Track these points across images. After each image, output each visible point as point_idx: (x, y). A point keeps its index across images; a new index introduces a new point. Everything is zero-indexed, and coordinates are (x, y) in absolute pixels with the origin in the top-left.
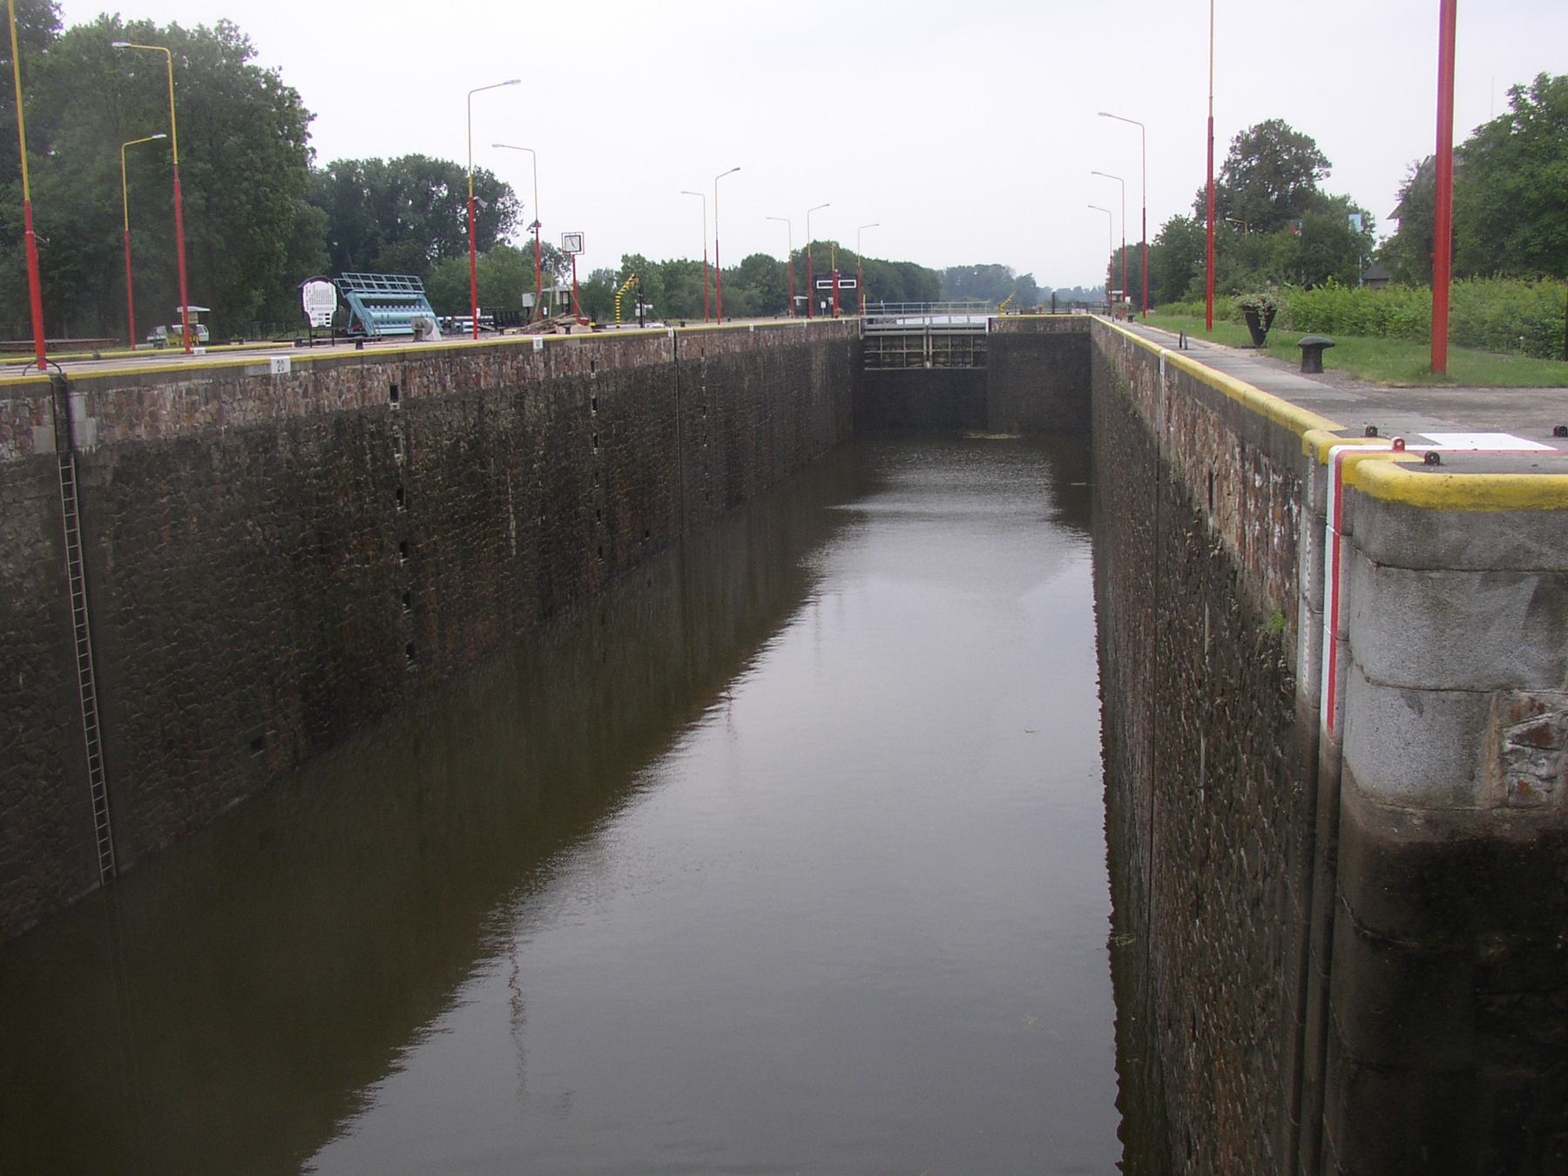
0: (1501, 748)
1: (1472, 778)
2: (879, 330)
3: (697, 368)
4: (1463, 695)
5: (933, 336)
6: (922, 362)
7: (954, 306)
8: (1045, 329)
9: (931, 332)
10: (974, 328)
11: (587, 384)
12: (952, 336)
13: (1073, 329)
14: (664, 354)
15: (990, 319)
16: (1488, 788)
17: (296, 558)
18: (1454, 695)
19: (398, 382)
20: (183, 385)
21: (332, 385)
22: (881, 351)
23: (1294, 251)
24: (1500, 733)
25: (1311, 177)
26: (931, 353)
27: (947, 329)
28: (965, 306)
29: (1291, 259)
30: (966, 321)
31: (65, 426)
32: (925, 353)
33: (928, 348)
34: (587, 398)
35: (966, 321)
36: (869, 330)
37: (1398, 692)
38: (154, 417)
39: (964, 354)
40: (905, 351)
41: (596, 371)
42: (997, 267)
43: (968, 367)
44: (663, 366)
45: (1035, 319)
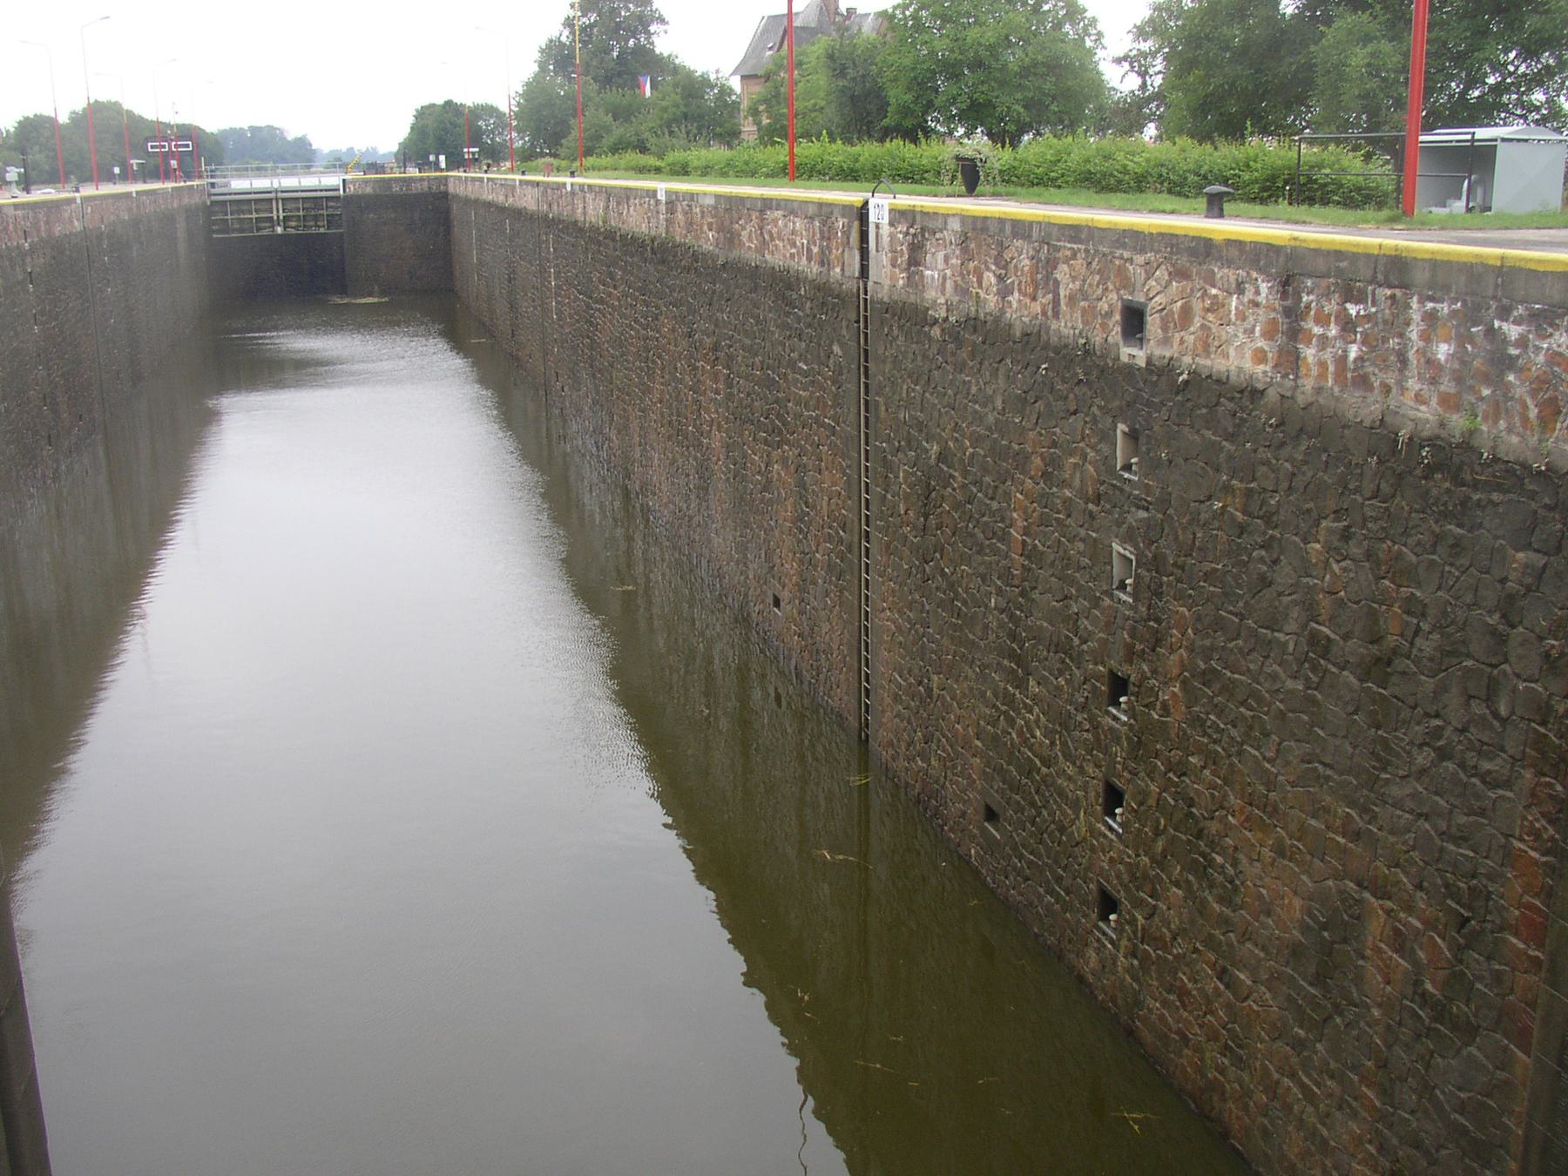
2: (225, 194)
3: (100, 237)
5: (283, 199)
6: (273, 227)
7: (236, 170)
8: (402, 190)
9: (280, 195)
10: (326, 190)
11: (23, 254)
12: (303, 198)
13: (430, 188)
14: (76, 223)
15: (344, 180)
22: (229, 217)
23: (677, 106)
25: (649, 34)
26: (281, 217)
27: (297, 191)
28: (247, 169)
29: (674, 114)
30: (317, 183)
32: (275, 218)
33: (278, 213)
34: (25, 271)
35: (317, 183)
36: (215, 195)
39: (316, 218)
40: (254, 215)
41: (29, 240)
42: (271, 128)
43: (322, 230)
44: (76, 235)
45: (390, 179)
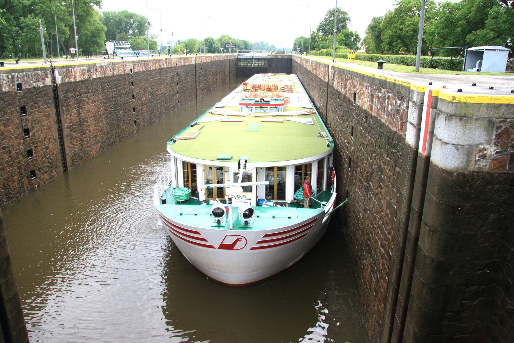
0: (476, 159)
1: (468, 166)
4: (468, 146)
16: (472, 167)
17: (109, 112)
18: (466, 147)
19: (132, 68)
20: (82, 68)
21: (117, 68)
24: (475, 155)
31: (54, 78)
37: (453, 146)
38: (75, 77)
